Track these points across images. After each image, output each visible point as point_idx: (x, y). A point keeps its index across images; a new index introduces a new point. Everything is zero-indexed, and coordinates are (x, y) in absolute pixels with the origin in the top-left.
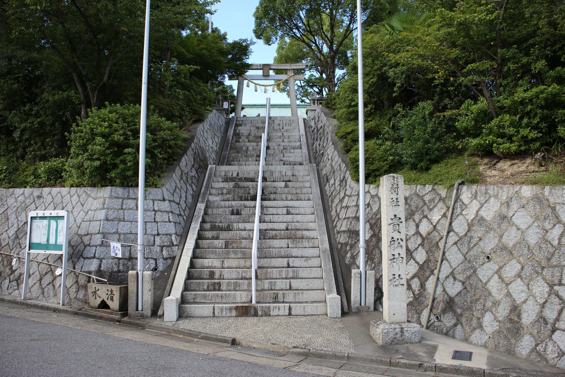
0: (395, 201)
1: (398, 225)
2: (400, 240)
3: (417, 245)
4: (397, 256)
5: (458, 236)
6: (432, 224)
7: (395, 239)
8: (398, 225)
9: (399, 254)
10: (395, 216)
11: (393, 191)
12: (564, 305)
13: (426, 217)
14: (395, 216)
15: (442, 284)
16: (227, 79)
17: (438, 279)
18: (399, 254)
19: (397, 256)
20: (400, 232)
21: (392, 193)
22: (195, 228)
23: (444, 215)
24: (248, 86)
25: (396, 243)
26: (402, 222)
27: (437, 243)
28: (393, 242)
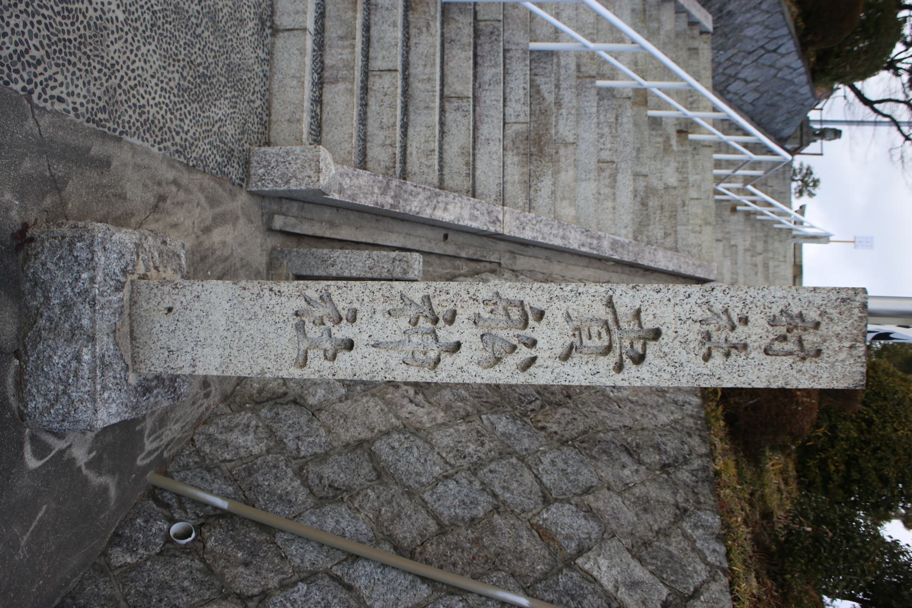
0: (733, 338)
1: (608, 349)
2: (524, 353)
4: (448, 335)
7: (538, 331)
8: (608, 349)
9: (457, 347)
11: (782, 330)
12: (165, 1)
14: (656, 334)
16: (113, 492)
17: (355, 558)
18: (457, 347)
19: (448, 335)
20: (566, 357)
21: (773, 322)
22: (215, 397)
25: (510, 335)
26: (619, 367)
28: (515, 314)
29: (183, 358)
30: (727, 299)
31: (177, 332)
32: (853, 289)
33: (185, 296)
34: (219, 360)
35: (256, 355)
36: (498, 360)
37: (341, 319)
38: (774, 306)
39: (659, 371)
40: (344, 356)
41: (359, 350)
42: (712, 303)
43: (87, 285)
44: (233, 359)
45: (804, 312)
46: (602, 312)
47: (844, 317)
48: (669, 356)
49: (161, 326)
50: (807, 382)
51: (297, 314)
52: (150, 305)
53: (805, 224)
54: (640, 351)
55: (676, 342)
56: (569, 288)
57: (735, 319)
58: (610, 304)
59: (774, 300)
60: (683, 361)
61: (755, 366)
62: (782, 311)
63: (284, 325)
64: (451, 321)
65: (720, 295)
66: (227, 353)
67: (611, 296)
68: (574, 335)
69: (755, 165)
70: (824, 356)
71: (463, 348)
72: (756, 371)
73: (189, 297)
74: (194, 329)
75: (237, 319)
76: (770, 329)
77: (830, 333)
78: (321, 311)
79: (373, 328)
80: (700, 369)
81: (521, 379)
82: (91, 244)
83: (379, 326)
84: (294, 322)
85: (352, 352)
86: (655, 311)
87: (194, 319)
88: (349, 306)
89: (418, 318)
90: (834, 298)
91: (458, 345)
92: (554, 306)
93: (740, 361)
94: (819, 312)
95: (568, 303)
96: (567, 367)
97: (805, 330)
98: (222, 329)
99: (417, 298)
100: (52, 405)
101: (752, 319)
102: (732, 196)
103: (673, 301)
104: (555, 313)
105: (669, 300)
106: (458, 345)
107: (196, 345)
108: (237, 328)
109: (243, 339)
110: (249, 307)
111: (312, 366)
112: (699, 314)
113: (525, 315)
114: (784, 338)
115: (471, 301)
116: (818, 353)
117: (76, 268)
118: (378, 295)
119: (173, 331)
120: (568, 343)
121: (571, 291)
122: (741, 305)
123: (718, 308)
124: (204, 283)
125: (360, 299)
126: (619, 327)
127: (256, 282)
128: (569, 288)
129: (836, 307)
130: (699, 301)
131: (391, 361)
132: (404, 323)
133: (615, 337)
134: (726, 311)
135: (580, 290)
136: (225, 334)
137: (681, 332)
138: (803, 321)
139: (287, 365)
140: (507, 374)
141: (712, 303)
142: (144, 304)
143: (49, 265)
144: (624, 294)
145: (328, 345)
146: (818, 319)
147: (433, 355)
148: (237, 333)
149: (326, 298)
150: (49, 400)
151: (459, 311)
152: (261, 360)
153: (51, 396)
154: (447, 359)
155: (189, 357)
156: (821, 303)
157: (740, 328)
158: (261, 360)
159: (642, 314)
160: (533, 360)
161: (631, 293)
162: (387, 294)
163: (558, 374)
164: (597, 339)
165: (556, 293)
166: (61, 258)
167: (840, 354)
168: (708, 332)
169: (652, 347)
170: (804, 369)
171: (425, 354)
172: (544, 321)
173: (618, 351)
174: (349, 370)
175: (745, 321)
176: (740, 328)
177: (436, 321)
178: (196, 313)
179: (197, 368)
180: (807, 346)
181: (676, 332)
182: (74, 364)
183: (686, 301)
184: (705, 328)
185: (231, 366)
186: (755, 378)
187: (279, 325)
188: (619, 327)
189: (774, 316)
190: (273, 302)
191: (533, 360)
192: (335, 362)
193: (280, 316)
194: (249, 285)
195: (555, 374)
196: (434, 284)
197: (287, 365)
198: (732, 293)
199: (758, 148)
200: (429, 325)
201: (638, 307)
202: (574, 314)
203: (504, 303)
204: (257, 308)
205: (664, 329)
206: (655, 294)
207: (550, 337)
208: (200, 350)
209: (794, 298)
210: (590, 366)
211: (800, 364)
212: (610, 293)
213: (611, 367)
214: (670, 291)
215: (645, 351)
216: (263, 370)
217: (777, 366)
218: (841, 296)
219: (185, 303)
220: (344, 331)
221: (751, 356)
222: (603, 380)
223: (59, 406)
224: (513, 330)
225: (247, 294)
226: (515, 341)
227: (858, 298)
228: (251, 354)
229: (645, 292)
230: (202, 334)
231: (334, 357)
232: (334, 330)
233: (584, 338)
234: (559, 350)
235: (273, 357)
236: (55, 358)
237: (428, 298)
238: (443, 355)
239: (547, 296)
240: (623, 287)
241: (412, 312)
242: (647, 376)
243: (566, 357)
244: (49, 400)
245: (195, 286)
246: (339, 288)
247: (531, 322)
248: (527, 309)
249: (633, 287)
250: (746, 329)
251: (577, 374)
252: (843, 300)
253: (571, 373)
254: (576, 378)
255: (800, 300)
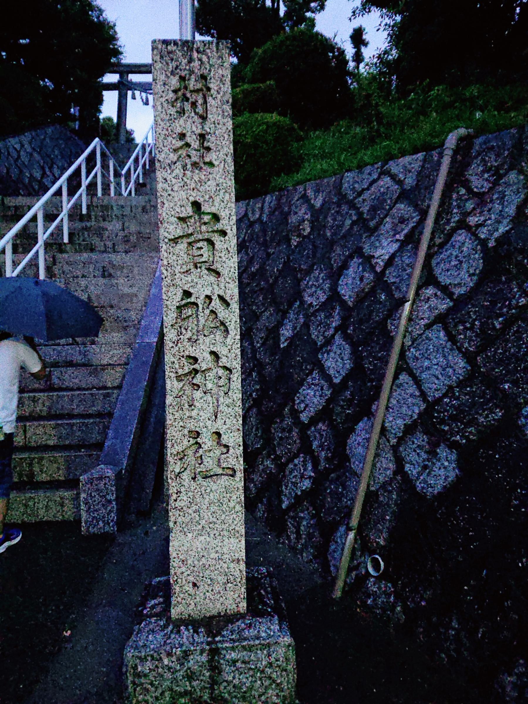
0: (195, 144)
1: (211, 243)
2: (216, 303)
3: (332, 331)
5: (450, 295)
6: (373, 268)
7: (200, 293)
8: (211, 243)
10: (196, 205)
11: (187, 106)
13: (359, 251)
14: (196, 205)
15: (395, 449)
21: (182, 112)
23: (412, 240)
24: (134, 98)
26: (224, 233)
27: (383, 323)
28: (189, 311)
29: (233, 570)
30: (166, 149)
31: (213, 576)
32: (153, 50)
33: (183, 573)
34: (232, 540)
35: (227, 509)
36: (223, 324)
37: (197, 443)
38: (169, 112)
39: (223, 202)
40: (225, 439)
41: (220, 427)
42: (170, 162)
43: (174, 659)
44: (231, 528)
45: (172, 88)
46: (182, 246)
47: (175, 57)
48: (212, 194)
49: (208, 592)
50: (226, 86)
51: (194, 479)
52: (191, 602)
53: (145, 142)
54: (210, 217)
55: (201, 190)
56: (164, 271)
57: (180, 143)
58: (175, 241)
59: (164, 113)
60: (215, 184)
61: (216, 127)
62: (173, 106)
63: (203, 488)
64: (195, 360)
65: (163, 155)
66: (226, 533)
67: (170, 240)
68: (200, 267)
69: (105, 166)
70: (206, 72)
71: (214, 349)
72: (220, 126)
73: (184, 569)
74: (209, 563)
75: (200, 527)
76: (186, 115)
77: (188, 67)
78: (191, 459)
79: (203, 417)
80: (221, 170)
81: (235, 306)
82: (140, 658)
83: (201, 413)
84: (201, 479)
85: (221, 432)
86: (178, 206)
87: (201, 563)
88: (187, 437)
89: (193, 384)
90: (160, 65)
91: (212, 353)
92: (180, 283)
93: (213, 139)
94: (172, 77)
95: (177, 272)
96: (224, 272)
97: (186, 88)
98: (208, 539)
99: (177, 385)
100: (274, 681)
101: (179, 130)
102: (132, 185)
103: (170, 192)
104: (185, 282)
105: (169, 195)
106: (212, 353)
107: (222, 560)
108: (207, 526)
109: (215, 520)
110: (190, 517)
111: (234, 463)
112: (178, 170)
113: (186, 305)
114: (194, 105)
115: (179, 345)
116: (204, 77)
117: (160, 670)
118: (177, 415)
119: (211, 580)
120: (206, 272)
121: (167, 270)
122: (170, 139)
123: (173, 157)
124: (171, 557)
125: (181, 429)
126: (192, 234)
127: (171, 514)
128: (164, 271)
129: (167, 64)
130: (169, 171)
131: (227, 403)
132: (198, 394)
133: (200, 237)
134: (175, 150)
135: (165, 263)
136: (212, 535)
137: (193, 185)
138: (179, 90)
139: (233, 483)
140: (232, 317)
141: (170, 162)
142: (191, 607)
143: (157, 694)
144: (167, 230)
145: (218, 452)
146: (177, 77)
147: (221, 372)
148: (211, 526)
149: (182, 456)
150: (271, 684)
151: (187, 353)
152: (232, 504)
153: (267, 683)
154: (224, 361)
155: (232, 565)
156: (164, 75)
157: (188, 139)
158: (232, 504)
159: (181, 216)
160: (221, 298)
161: (166, 225)
162: (176, 408)
163: (230, 278)
164: (202, 250)
165: (169, 281)
166: (152, 684)
167: (204, 60)
168: (192, 165)
169: (205, 208)
170: (216, 88)
171: (220, 378)
172: (191, 290)
173: (210, 234)
174: (236, 434)
175: (182, 136)
176: (188, 139)
177: (196, 371)
178: (196, 562)
179: (240, 558)
180: (199, 86)
181: (193, 189)
182: (239, 664)
183: (169, 182)
184: (189, 166)
185: (236, 529)
186: (224, 128)
187: (203, 492)
188: (192, 234)
189: (177, 112)
190: (185, 498)
191: (221, 298)
192: (230, 445)
193: (196, 491)
194: (172, 519)
195: (230, 281)
196: (167, 373)
197: (233, 483)
198: (161, 146)
199: (91, 161)
200: (199, 376)
201: (176, 219)
202: (185, 268)
203: (179, 320)
204: (190, 511)
205: (192, 199)
206: (166, 206)
207: (203, 286)
208: (225, 556)
209: (162, 97)
210: (222, 255)
211: (212, 91)
212: (166, 240)
213: (222, 239)
214: (163, 194)
215: (209, 214)
216: (239, 503)
217: (215, 109)
218: (159, 60)
219: (189, 572)
220: (207, 441)
221: (208, 130)
222: (233, 245)
223: (274, 676)
224: (199, 313)
225: (180, 520)
226: (207, 312)
227: (160, 46)
228: (227, 513)
229: (164, 214)
230: (213, 555)
231: (227, 447)
232: (205, 447)
233: (203, 259)
234: (212, 278)
235: (228, 495)
236: (234, 681)
237: (179, 378)
238: (221, 364)
239: (172, 289)
240: (162, 231)
241: (188, 389)
242: (227, 212)
243: (218, 274)
244: (271, 684)
245: (175, 565)
246: (173, 445)
247: (192, 300)
248: (184, 302)
249: (161, 223)
250: (188, 134)
251: (229, 263)
252: (162, 57)
253: (228, 269)
254: (232, 265)
255: (163, 92)
